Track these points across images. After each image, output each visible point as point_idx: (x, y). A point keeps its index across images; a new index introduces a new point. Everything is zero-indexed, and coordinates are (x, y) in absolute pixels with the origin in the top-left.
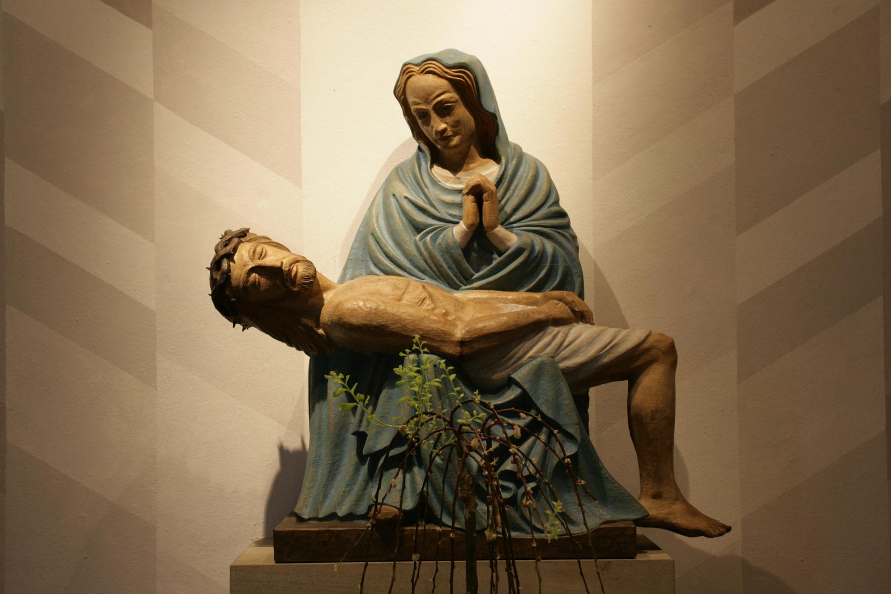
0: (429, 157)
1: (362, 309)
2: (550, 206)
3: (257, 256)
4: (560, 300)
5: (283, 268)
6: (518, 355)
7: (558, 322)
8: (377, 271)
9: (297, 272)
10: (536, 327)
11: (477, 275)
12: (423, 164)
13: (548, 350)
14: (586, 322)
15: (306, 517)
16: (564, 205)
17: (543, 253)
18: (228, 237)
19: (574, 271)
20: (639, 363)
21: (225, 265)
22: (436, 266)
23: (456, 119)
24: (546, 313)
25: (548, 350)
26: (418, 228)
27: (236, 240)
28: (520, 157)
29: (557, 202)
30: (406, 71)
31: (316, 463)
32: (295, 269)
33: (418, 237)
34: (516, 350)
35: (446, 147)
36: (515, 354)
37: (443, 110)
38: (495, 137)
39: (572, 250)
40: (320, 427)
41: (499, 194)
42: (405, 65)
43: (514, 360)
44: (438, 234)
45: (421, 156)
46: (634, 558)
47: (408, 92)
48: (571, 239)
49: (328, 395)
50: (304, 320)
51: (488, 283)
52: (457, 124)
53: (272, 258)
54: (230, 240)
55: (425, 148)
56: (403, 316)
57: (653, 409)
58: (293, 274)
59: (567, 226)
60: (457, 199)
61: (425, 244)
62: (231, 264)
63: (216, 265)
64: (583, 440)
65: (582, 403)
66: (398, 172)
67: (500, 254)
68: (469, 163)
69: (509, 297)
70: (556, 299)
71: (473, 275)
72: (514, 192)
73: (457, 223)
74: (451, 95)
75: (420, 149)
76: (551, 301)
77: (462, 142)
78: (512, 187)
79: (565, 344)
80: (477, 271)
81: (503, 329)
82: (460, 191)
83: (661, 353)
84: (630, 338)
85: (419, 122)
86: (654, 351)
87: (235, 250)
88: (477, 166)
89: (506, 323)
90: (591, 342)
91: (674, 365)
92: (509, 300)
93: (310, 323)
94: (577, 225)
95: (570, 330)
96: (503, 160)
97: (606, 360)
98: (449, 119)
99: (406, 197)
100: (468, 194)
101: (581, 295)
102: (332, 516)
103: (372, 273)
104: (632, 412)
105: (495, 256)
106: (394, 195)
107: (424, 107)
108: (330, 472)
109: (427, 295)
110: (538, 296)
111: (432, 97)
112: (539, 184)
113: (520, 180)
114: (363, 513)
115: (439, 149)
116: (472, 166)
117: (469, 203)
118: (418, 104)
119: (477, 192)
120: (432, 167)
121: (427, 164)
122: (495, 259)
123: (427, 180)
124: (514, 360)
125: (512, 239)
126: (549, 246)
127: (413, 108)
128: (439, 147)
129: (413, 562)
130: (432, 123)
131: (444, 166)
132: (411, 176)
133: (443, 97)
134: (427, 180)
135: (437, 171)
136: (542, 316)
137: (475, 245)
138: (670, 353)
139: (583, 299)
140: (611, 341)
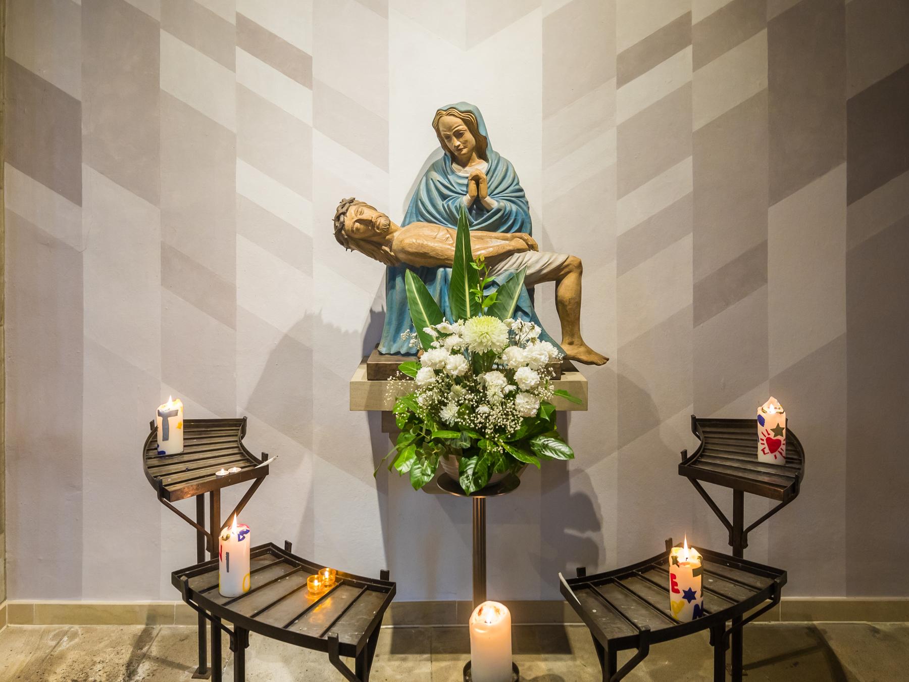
0: (450, 159)
1: (415, 244)
2: (514, 186)
3: (358, 214)
4: (521, 238)
5: (373, 221)
6: (498, 269)
7: (520, 251)
8: (422, 220)
9: (379, 224)
10: (509, 254)
11: (475, 223)
12: (447, 162)
13: (515, 266)
14: (535, 250)
15: (384, 353)
16: (522, 185)
17: (511, 212)
18: (344, 203)
19: (527, 220)
20: (562, 273)
21: (342, 219)
22: (454, 218)
23: (465, 139)
24: (513, 246)
25: (515, 266)
26: (444, 197)
27: (348, 205)
28: (499, 159)
29: (518, 184)
30: (439, 114)
31: (390, 323)
32: (379, 220)
33: (444, 202)
34: (497, 266)
35: (460, 154)
36: (496, 268)
37: (459, 135)
38: (431, 257)
39: (525, 208)
40: (392, 304)
41: (488, 179)
42: (438, 111)
43: (495, 272)
44: (455, 201)
45: (446, 158)
46: (560, 380)
47: (440, 125)
48: (526, 204)
49: (363, 340)
50: (384, 247)
51: (482, 227)
52: (465, 142)
53: (368, 215)
54: (344, 205)
55: (448, 154)
56: (437, 248)
57: (570, 298)
58: (378, 224)
59: (523, 197)
60: (465, 182)
61: (448, 206)
62: (345, 218)
63: (338, 218)
64: (532, 315)
65: (531, 292)
66: (434, 167)
67: (488, 212)
68: (471, 162)
69: (493, 236)
70: (519, 238)
71: (473, 223)
72: (495, 179)
73: (466, 195)
74: (463, 127)
75: (445, 154)
76: (516, 239)
77: (468, 152)
78: (495, 176)
79: (523, 263)
80: (476, 220)
81: (491, 255)
82: (467, 178)
83: (574, 267)
84: (559, 260)
85: (446, 141)
86: (571, 266)
87: (347, 210)
88: (476, 164)
89: (492, 252)
90: (537, 262)
91: (581, 273)
92: (493, 237)
93: (387, 249)
94: (529, 196)
95: (526, 255)
96: (490, 162)
97: (545, 271)
98: (461, 140)
99: (438, 181)
100: (471, 180)
101: (530, 234)
102: (398, 353)
103: (419, 221)
104: (558, 299)
105: (485, 212)
106: (432, 179)
107: (448, 133)
108: (397, 329)
109: (449, 236)
110: (509, 235)
111: (453, 128)
112: (508, 174)
113: (498, 172)
114: (414, 353)
115: (456, 156)
116: (473, 164)
117: (473, 185)
118: (445, 131)
119: (477, 179)
120: (452, 164)
121: (449, 162)
122: (485, 214)
123: (449, 171)
124: (495, 272)
125: (493, 203)
126: (514, 208)
127: (442, 133)
128: (456, 154)
129: (430, 474)
130: (452, 141)
131: (458, 164)
132: (441, 169)
133: (456, 129)
134: (449, 171)
135: (455, 166)
136: (511, 248)
137: (475, 206)
138: (580, 266)
139: (531, 237)
140: (548, 262)
